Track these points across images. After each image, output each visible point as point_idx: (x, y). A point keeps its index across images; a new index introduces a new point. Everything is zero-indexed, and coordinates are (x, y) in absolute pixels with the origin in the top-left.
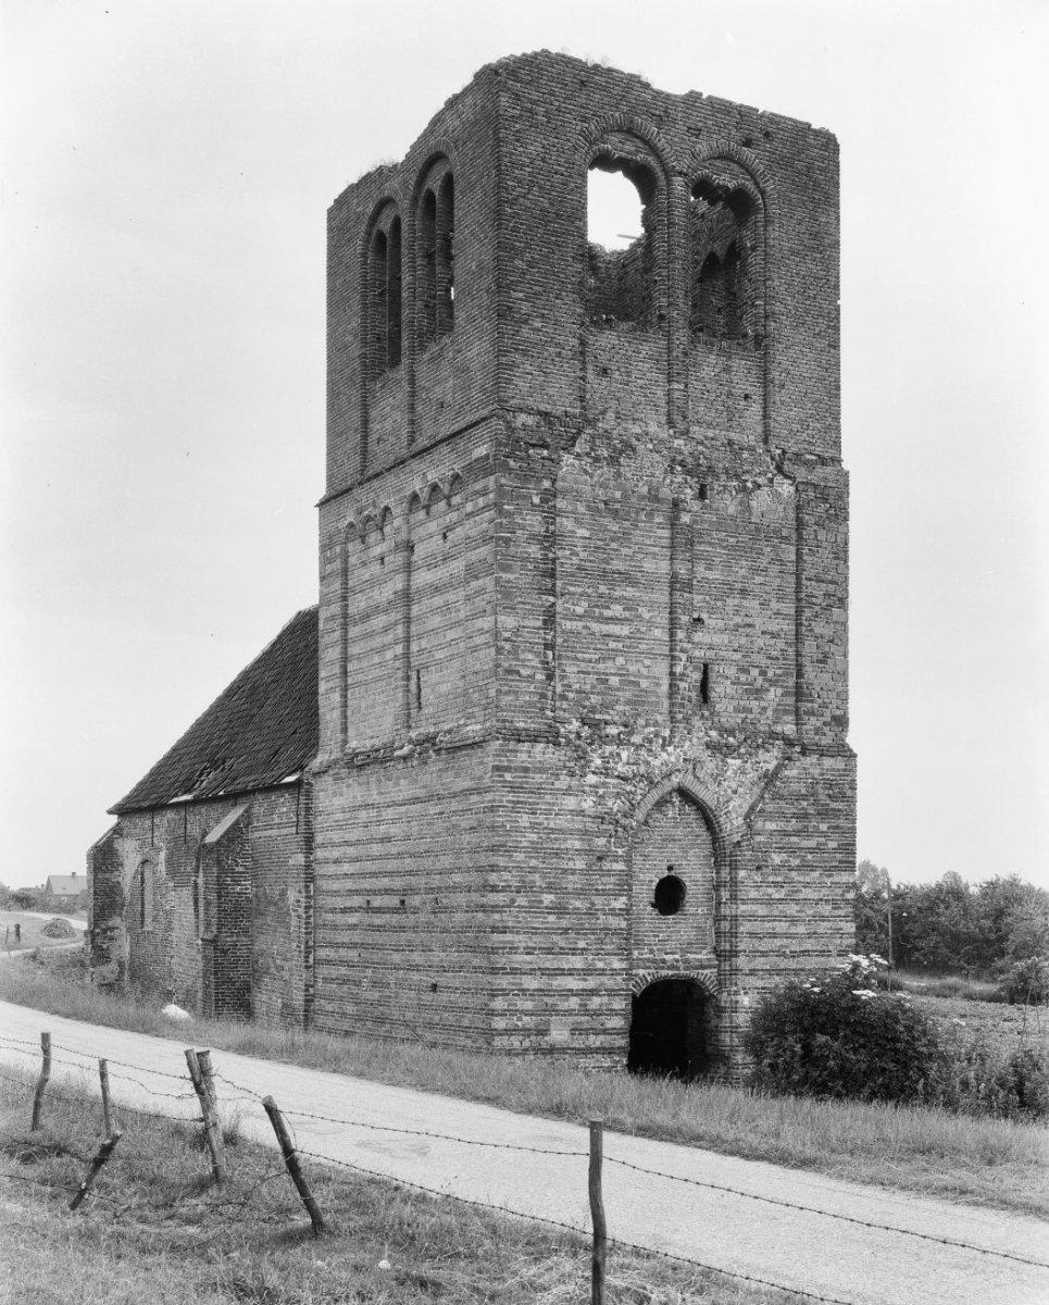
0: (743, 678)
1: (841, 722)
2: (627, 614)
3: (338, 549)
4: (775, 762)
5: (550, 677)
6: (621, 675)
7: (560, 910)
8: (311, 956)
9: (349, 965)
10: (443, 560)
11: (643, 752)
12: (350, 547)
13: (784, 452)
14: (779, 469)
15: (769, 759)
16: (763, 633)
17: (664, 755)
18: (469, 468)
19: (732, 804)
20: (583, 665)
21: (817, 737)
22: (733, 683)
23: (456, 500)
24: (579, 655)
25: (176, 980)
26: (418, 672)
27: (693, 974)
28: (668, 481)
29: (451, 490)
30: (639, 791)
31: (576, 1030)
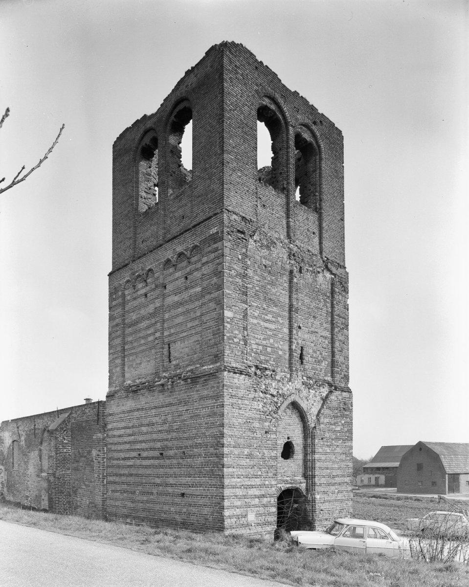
0: (314, 355)
1: (346, 378)
2: (274, 319)
3: (120, 293)
4: (326, 393)
5: (246, 344)
6: (272, 348)
7: (250, 456)
8: (105, 480)
9: (128, 484)
10: (185, 289)
11: (280, 384)
12: (127, 292)
13: (328, 259)
14: (327, 267)
15: (325, 391)
16: (321, 336)
17: (288, 385)
18: (204, 242)
19: (312, 410)
20: (257, 340)
21: (340, 383)
22: (311, 357)
23: (193, 259)
24: (256, 336)
25: (30, 491)
26: (169, 345)
27: (298, 486)
28: (288, 262)
29: (191, 254)
30: (279, 402)
31: (258, 515)
